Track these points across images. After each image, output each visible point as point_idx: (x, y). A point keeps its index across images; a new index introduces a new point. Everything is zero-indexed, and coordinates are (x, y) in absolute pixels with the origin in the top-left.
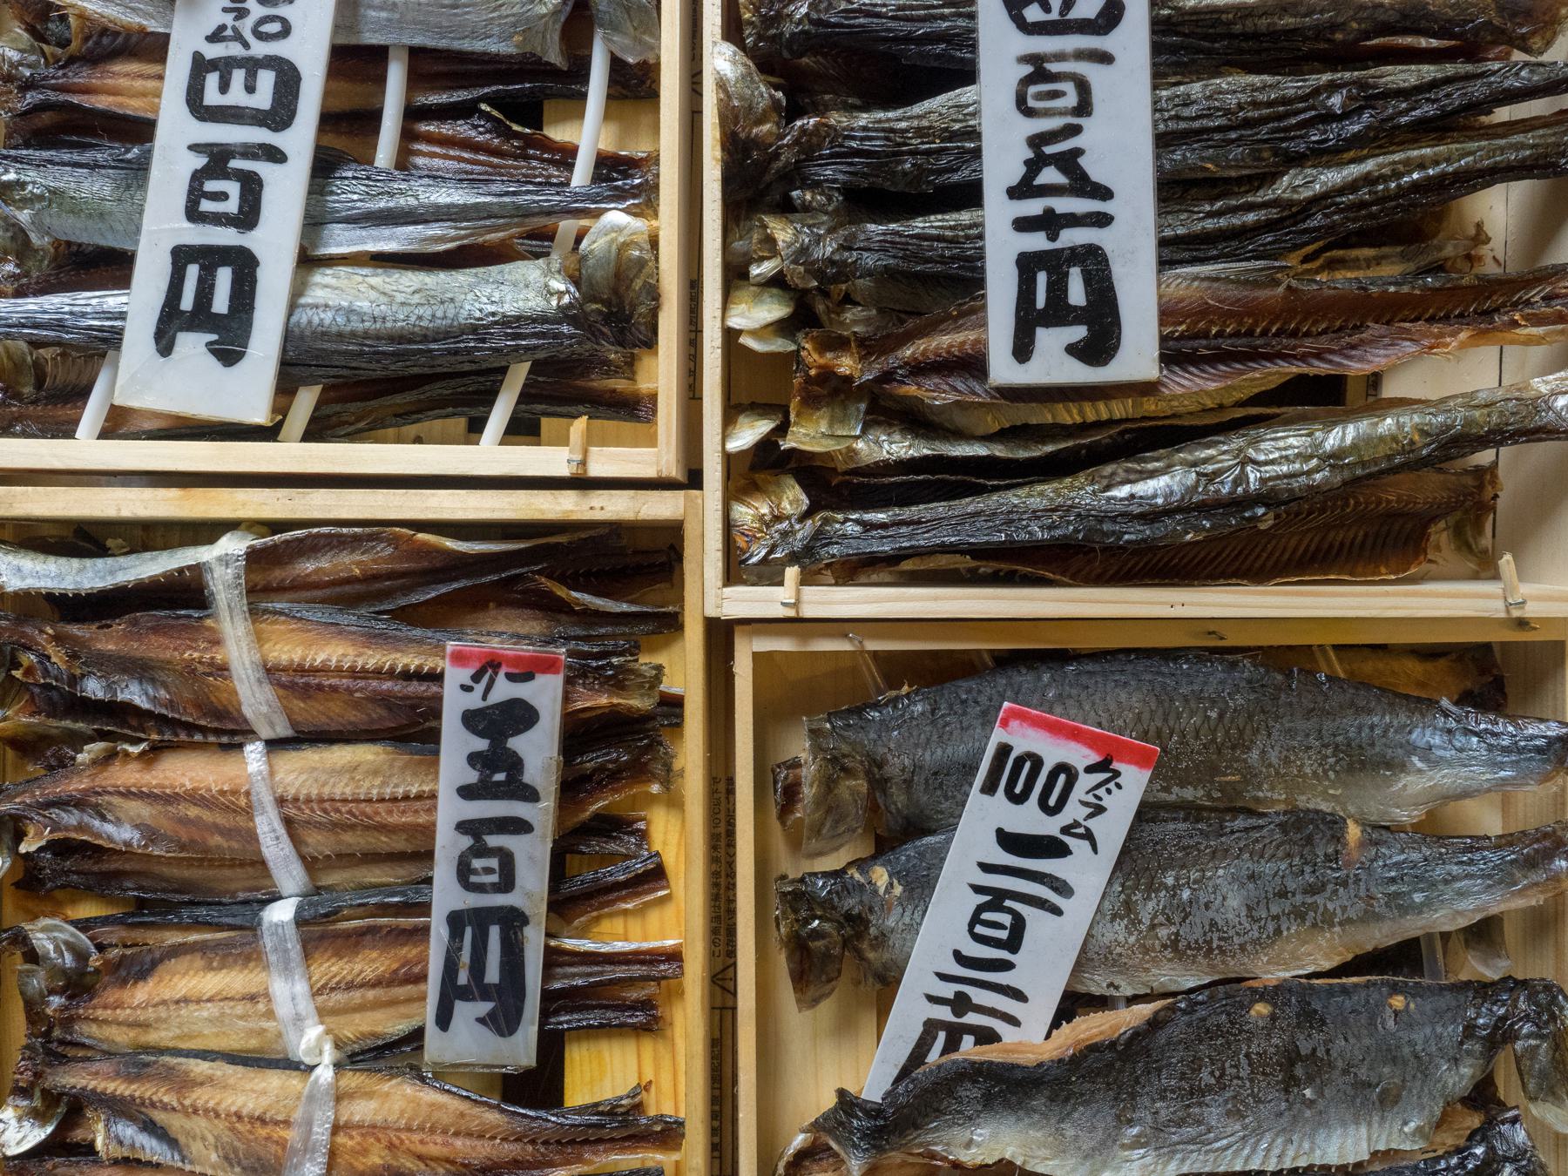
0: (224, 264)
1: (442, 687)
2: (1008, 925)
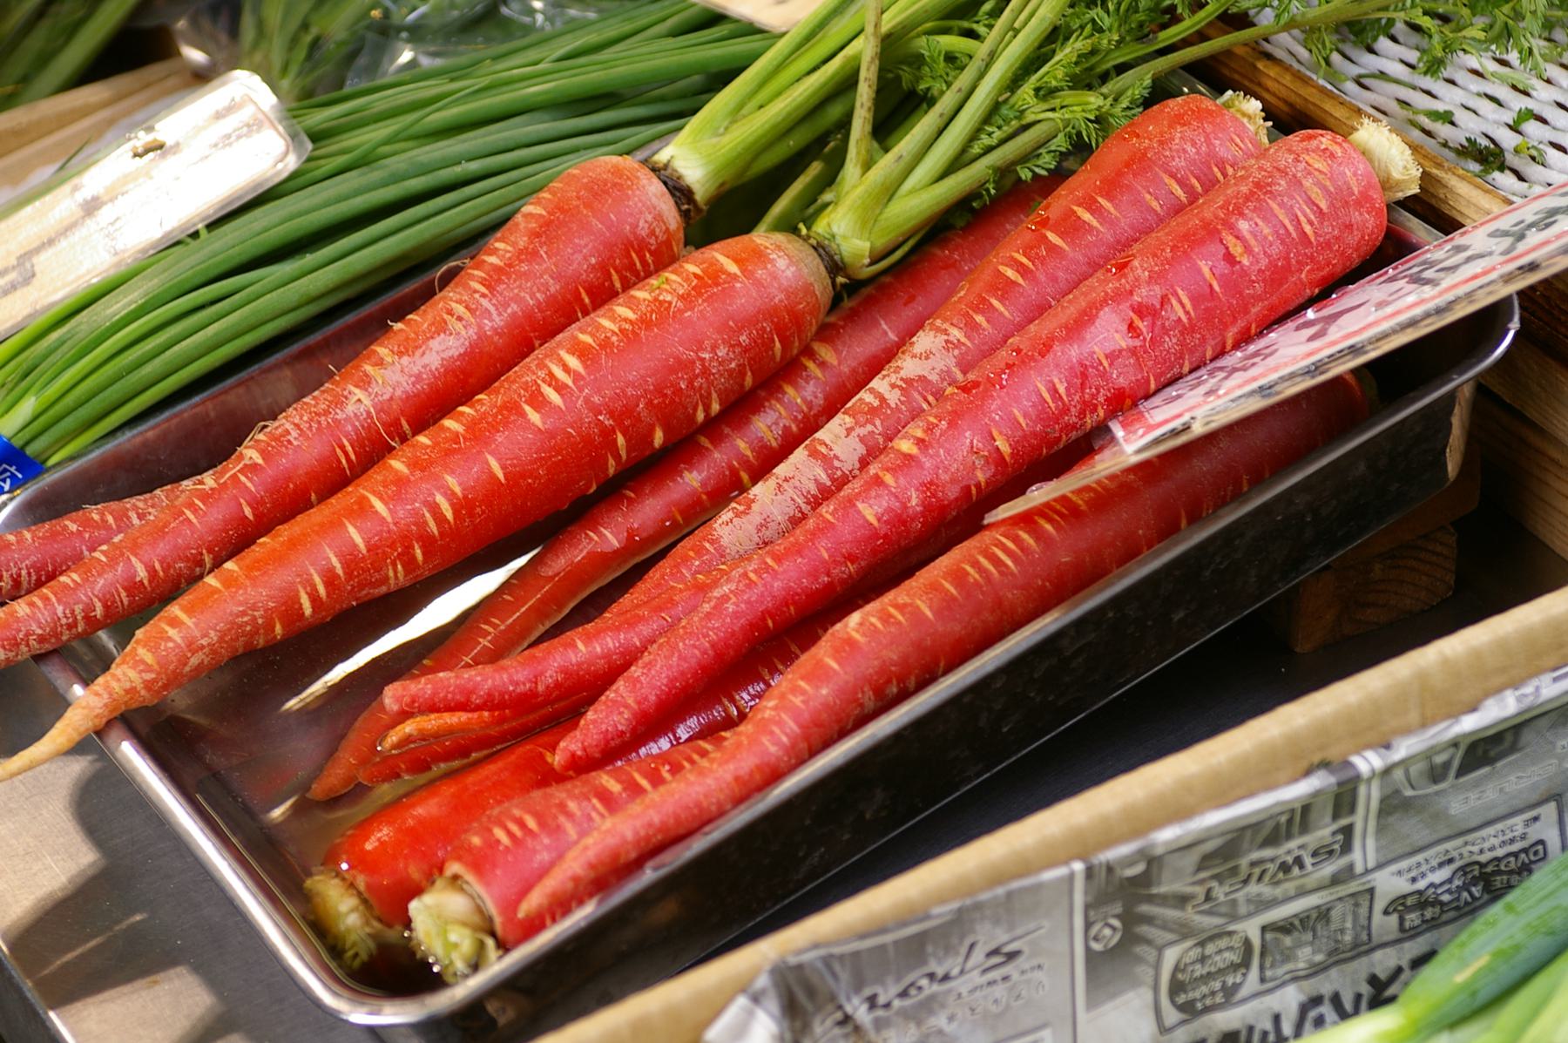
1: (1335, 1023)
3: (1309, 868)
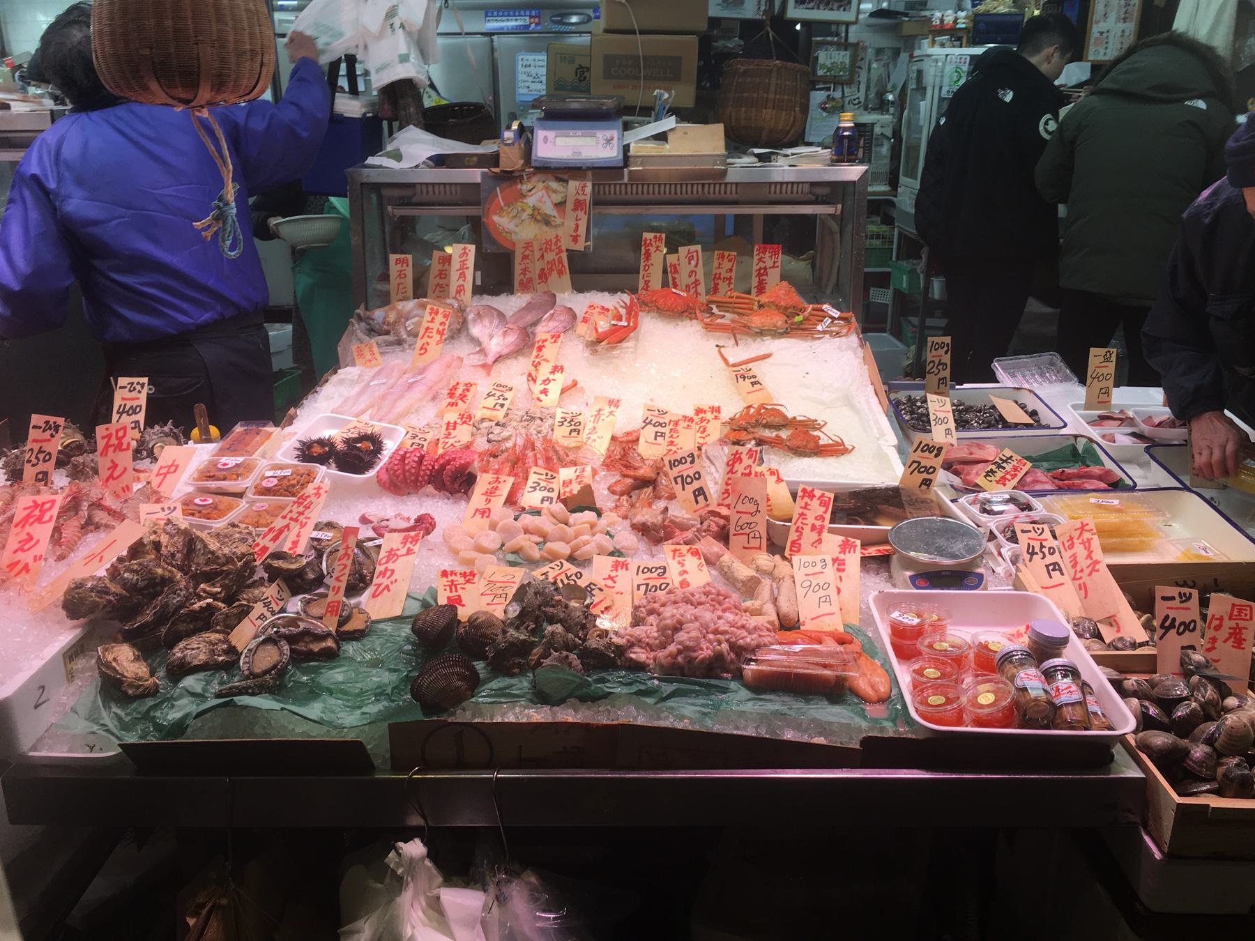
0: (1161, 860)
2: (31, 430)
3: (829, 562)
